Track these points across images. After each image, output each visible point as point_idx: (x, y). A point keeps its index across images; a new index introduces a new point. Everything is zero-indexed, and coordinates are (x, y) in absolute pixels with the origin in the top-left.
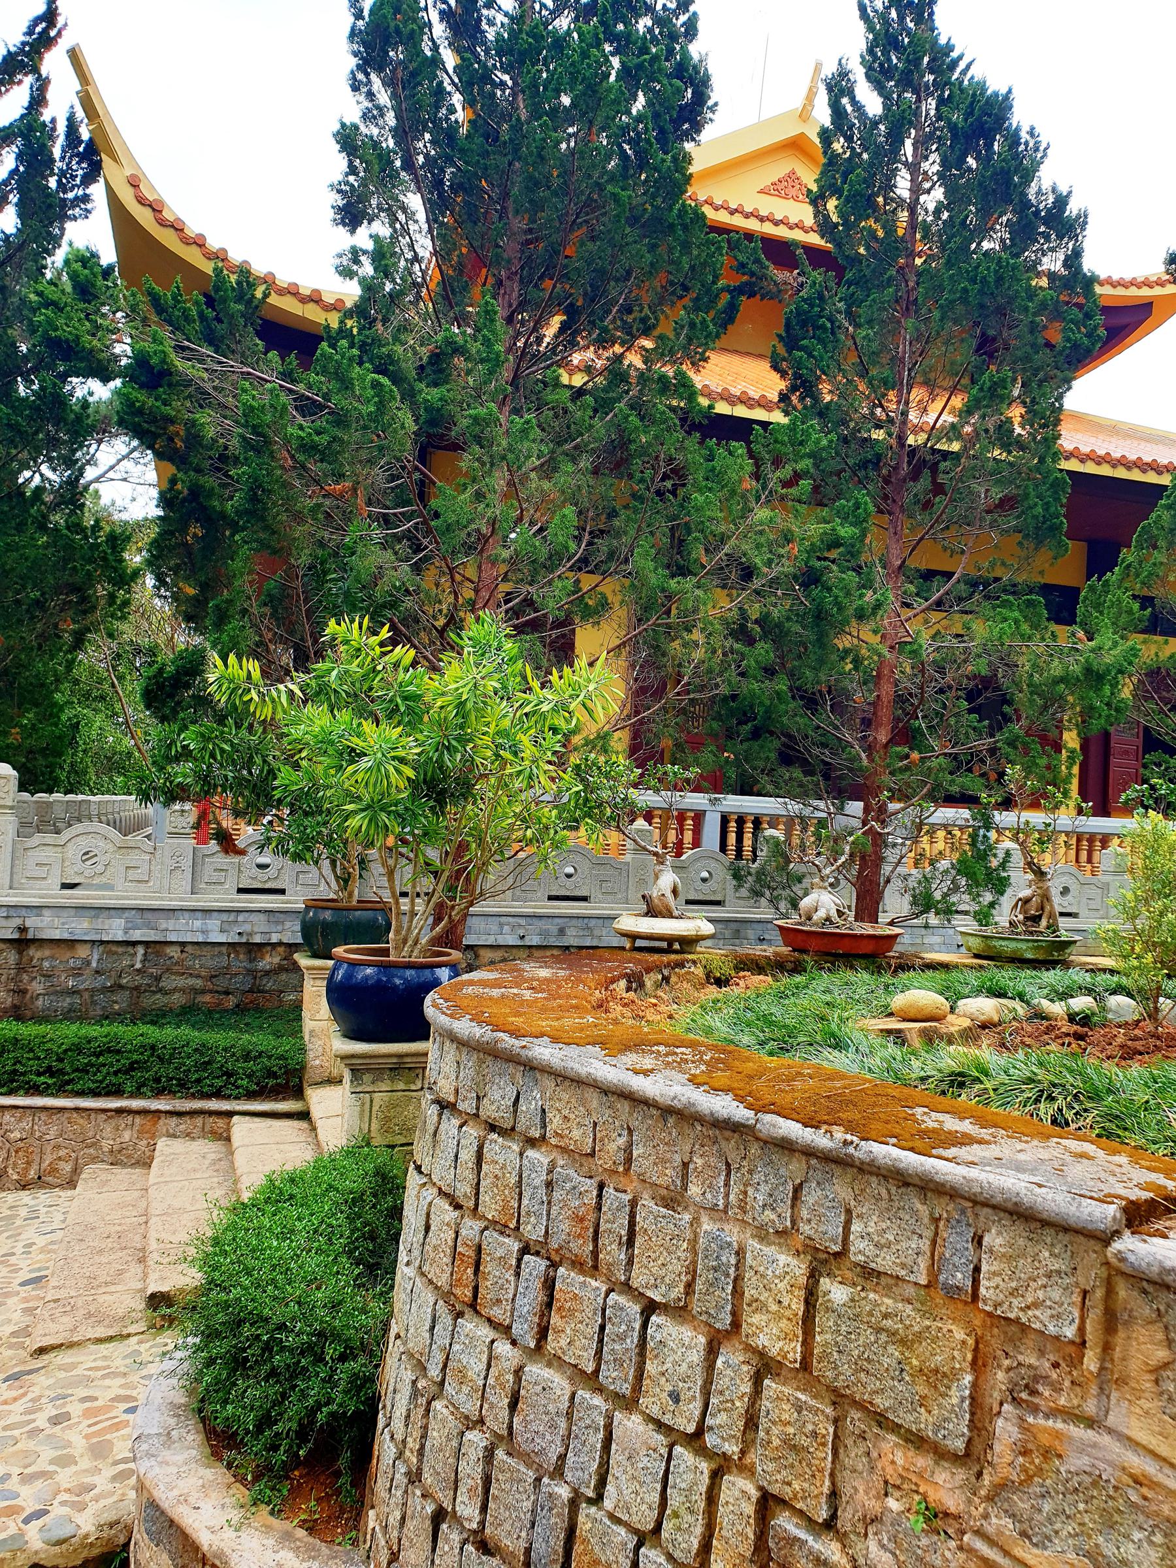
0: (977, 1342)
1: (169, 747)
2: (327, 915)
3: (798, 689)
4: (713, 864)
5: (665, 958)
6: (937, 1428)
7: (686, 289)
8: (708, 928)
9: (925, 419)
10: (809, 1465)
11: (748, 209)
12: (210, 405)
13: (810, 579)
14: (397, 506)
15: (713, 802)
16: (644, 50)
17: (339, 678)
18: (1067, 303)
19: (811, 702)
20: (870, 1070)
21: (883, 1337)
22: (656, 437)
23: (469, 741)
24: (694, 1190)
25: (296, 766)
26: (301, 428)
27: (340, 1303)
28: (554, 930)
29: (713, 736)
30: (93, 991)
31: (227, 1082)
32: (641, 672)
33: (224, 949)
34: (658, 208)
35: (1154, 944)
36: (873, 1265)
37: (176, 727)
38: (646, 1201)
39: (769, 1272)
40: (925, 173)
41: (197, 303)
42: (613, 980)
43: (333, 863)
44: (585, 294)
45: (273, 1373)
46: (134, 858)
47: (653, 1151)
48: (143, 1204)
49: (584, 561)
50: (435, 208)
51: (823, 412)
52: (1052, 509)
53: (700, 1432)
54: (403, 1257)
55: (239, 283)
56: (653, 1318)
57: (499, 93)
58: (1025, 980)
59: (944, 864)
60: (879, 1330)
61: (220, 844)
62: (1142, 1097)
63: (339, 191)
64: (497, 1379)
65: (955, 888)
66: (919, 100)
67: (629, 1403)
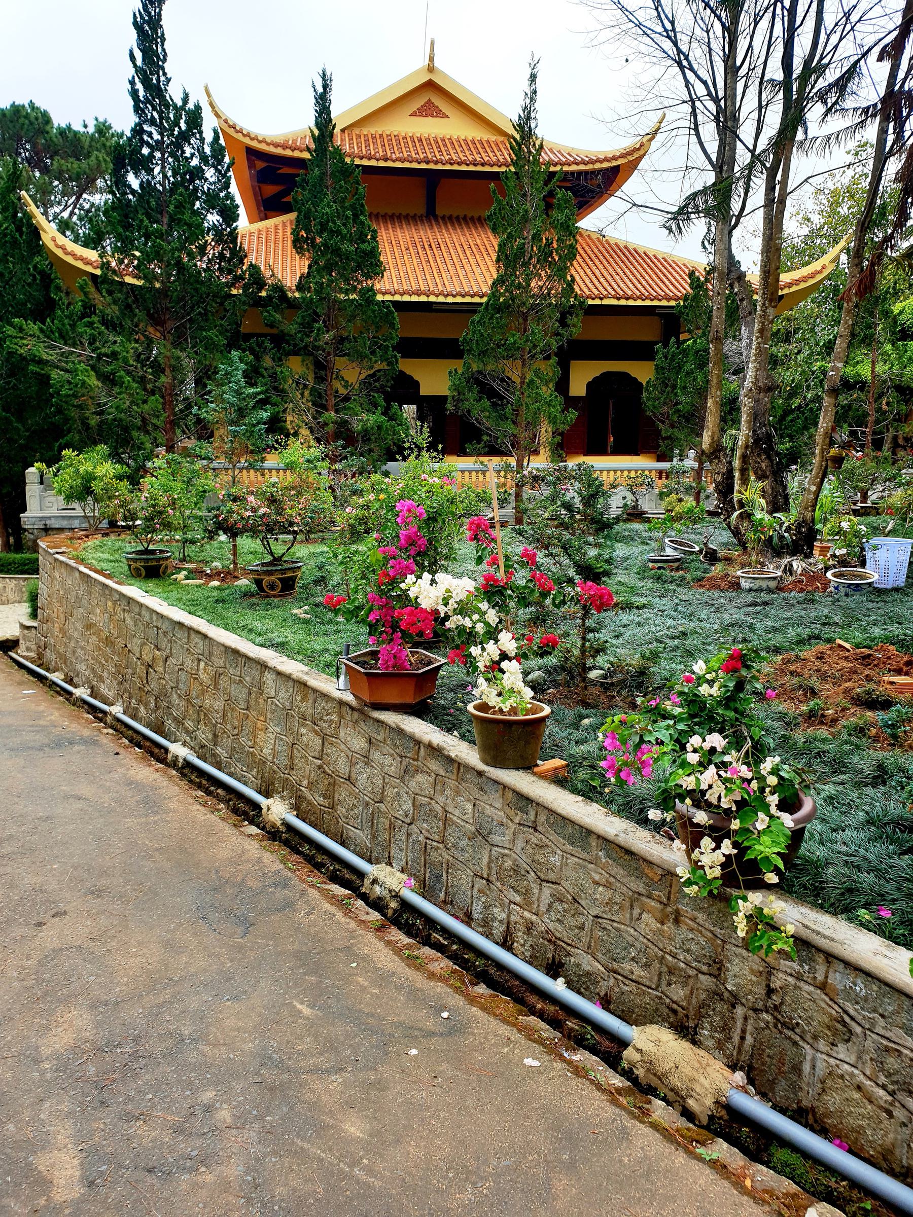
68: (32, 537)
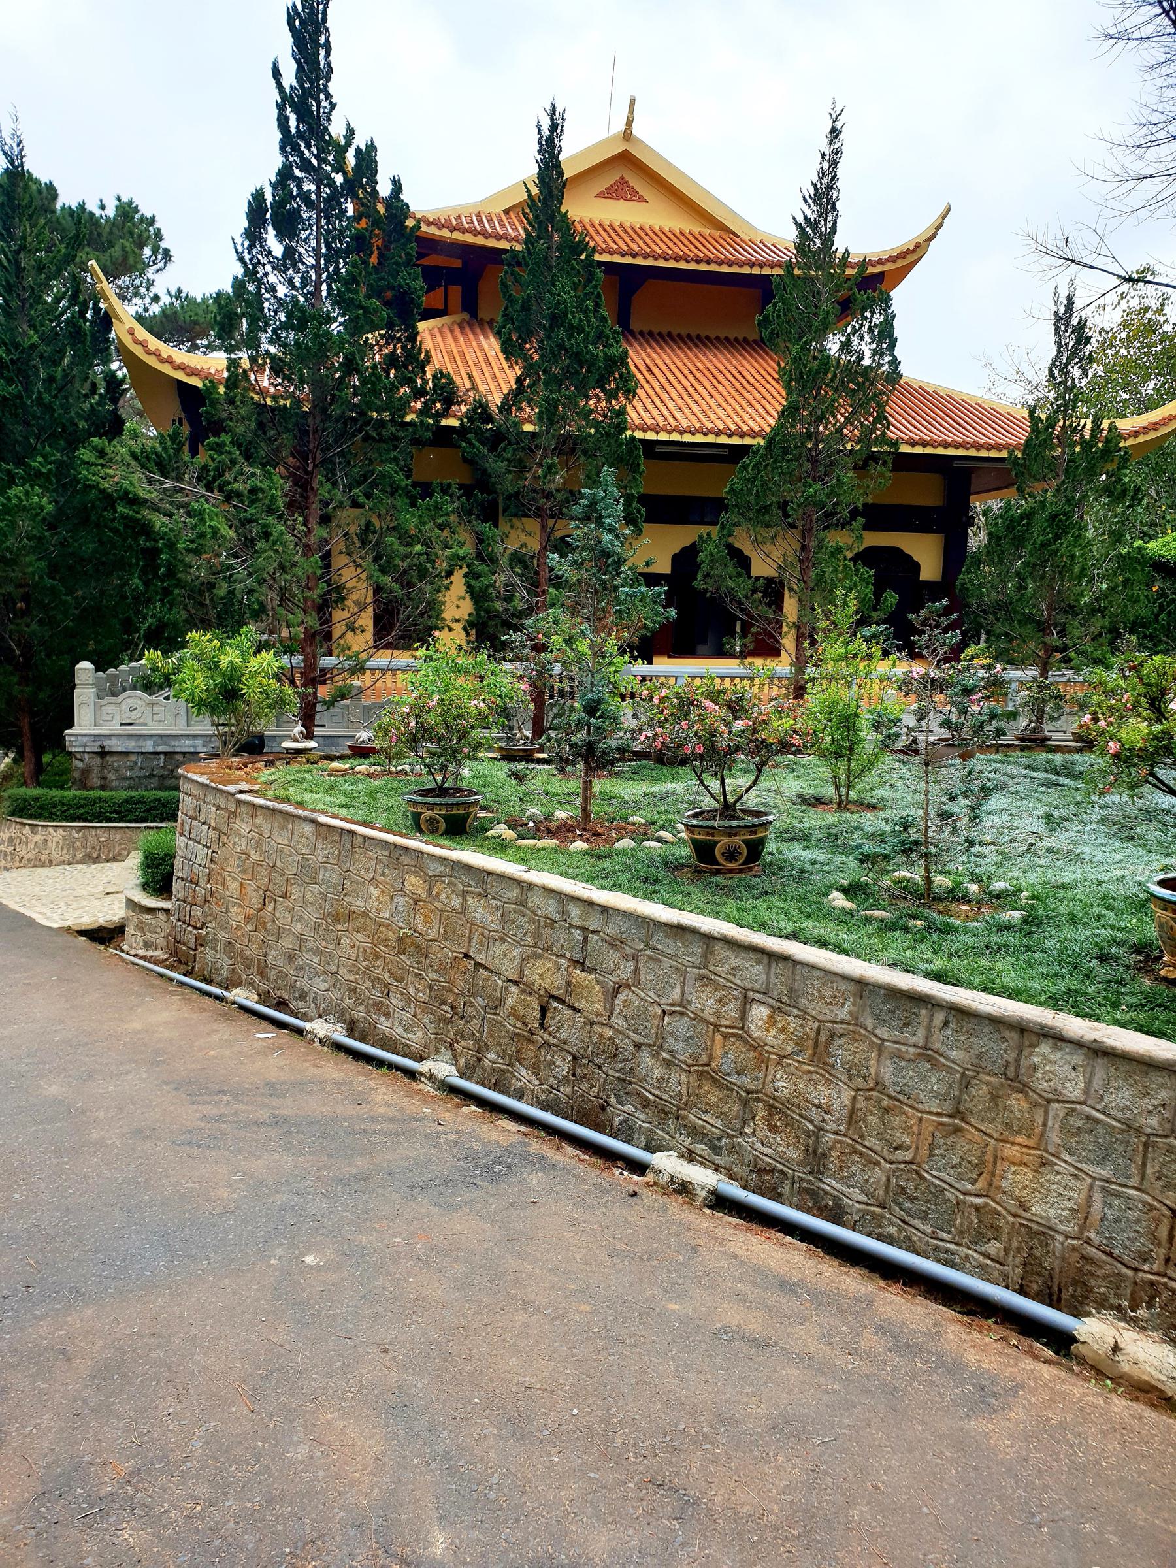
30: (140, 778)
68: (80, 764)
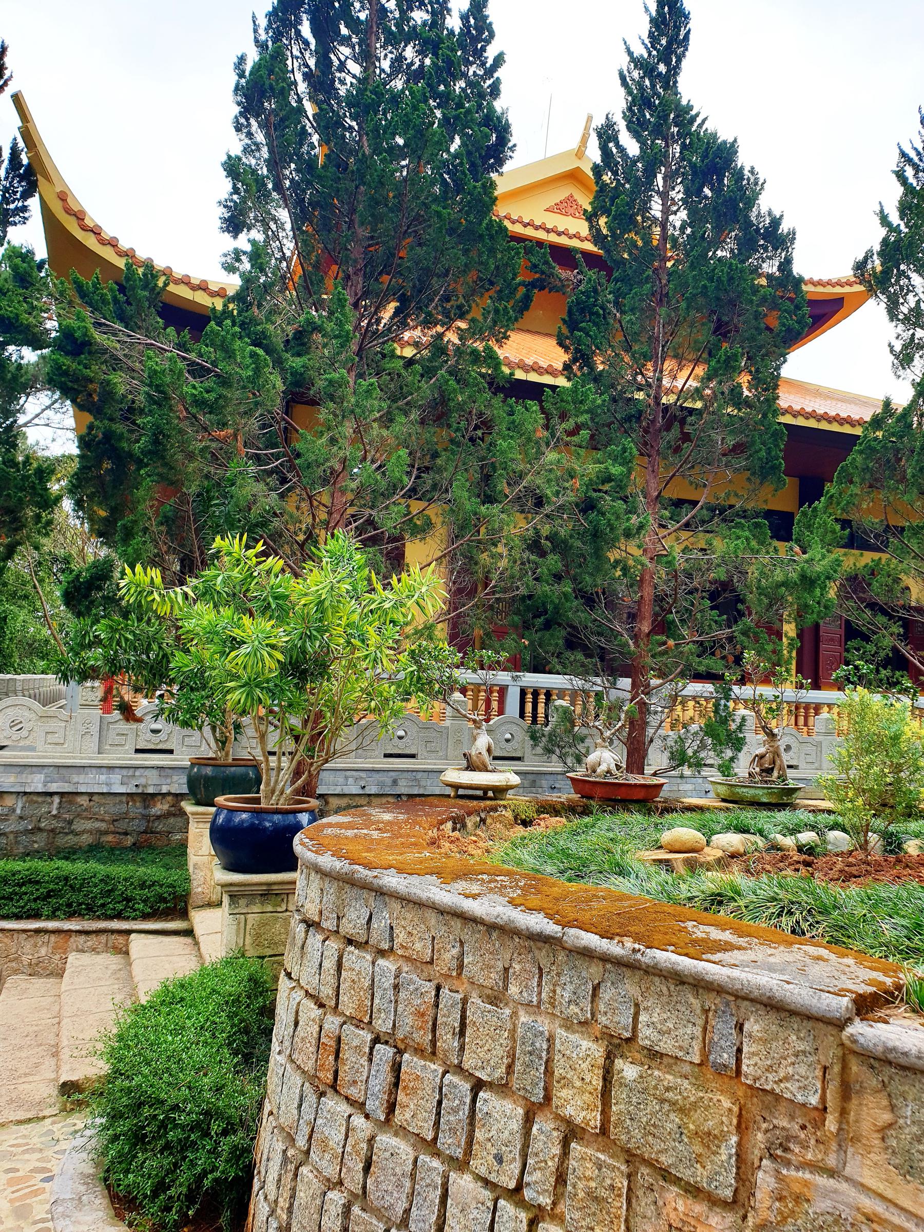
0: (740, 1109)
1: (84, 636)
2: (209, 771)
3: (580, 590)
4: (515, 728)
5: (483, 804)
6: (711, 1180)
7: (492, 283)
8: (515, 780)
9: (675, 383)
10: (608, 1213)
11: (538, 223)
12: (121, 369)
13: (588, 506)
14: (266, 448)
15: (515, 679)
16: (460, 105)
17: (224, 582)
18: (782, 297)
19: (590, 601)
20: (648, 892)
21: (666, 1106)
22: (470, 397)
23: (326, 631)
24: (513, 990)
25: (187, 651)
26: (194, 387)
27: (223, 1086)
28: (389, 781)
29: (515, 626)
30: (17, 833)
31: (126, 906)
32: (458, 577)
33: (124, 799)
34: (471, 222)
35: (864, 791)
36: (657, 1048)
37: (89, 621)
38: (475, 999)
39: (574, 1055)
40: (673, 199)
41: (111, 290)
42: (442, 822)
43: (214, 729)
44: (414, 286)
45: (167, 1147)
46: (53, 725)
47: (480, 960)
48: (57, 1008)
49: (413, 490)
50: (298, 220)
51: (597, 378)
52: (773, 453)
53: (519, 1188)
54: (275, 1046)
55: (145, 275)
56: (481, 1094)
57: (348, 135)
58: (763, 819)
59: (694, 728)
60: (662, 1101)
61: (122, 713)
62: (860, 911)
63: (225, 206)
64: (353, 1147)
65: (703, 746)
66: (667, 146)
67: (462, 1165)
